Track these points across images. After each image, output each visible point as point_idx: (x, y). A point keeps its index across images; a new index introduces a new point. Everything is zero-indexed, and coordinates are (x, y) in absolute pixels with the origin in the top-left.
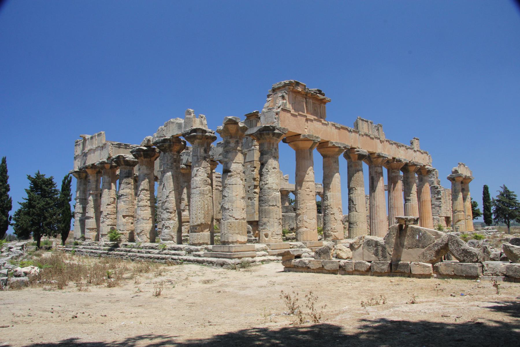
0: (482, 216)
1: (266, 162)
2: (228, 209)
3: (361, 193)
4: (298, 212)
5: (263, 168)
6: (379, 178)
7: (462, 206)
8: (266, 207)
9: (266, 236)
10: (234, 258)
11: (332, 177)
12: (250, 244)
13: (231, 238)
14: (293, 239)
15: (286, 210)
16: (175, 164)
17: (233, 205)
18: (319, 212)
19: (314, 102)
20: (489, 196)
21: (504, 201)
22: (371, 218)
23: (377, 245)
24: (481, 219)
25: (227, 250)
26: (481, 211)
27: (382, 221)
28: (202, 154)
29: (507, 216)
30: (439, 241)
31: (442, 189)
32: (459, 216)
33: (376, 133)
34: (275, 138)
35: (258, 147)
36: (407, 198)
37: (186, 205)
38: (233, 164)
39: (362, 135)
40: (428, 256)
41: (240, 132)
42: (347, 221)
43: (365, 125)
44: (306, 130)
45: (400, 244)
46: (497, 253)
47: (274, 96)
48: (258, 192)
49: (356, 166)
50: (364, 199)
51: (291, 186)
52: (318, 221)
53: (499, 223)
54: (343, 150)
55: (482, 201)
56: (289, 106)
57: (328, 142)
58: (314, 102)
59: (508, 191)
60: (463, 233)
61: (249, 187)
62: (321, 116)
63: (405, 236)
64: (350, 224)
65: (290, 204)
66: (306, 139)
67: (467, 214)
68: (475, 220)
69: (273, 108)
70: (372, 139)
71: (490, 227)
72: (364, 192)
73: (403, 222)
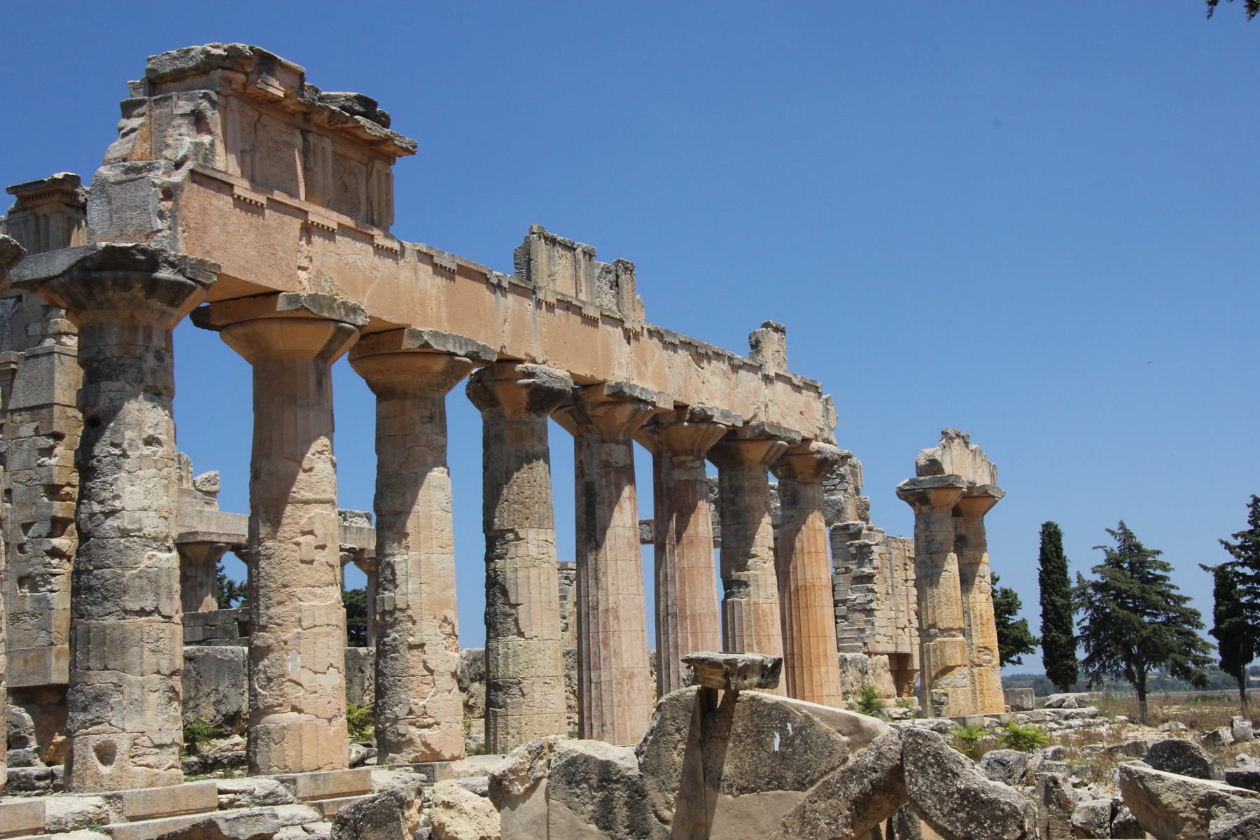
0: (1039, 650)
1: (114, 411)
3: (543, 550)
4: (261, 639)
5: (97, 439)
6: (619, 491)
7: (957, 611)
8: (110, 621)
12: (18, 800)
14: (236, 763)
15: (203, 630)
18: (356, 636)
20: (1063, 569)
21: (1124, 587)
22: (583, 662)
23: (609, 781)
24: (1033, 663)
26: (1035, 629)
27: (631, 676)
29: (1135, 650)
31: (879, 538)
32: (948, 651)
33: (608, 300)
34: (157, 304)
35: (72, 342)
36: (735, 574)
39: (550, 307)
40: (822, 824)
42: (480, 677)
43: (563, 263)
44: (302, 275)
45: (706, 770)
46: (1097, 804)
47: (157, 112)
48: (72, 552)
49: (520, 437)
50: (555, 579)
51: (228, 521)
52: (349, 681)
53: (1105, 679)
54: (469, 367)
55: (1038, 588)
56: (225, 163)
57: (399, 330)
58: (341, 149)
59: (1138, 547)
60: (962, 721)
61: (26, 527)
62: (370, 213)
64: (490, 689)
65: (224, 603)
66: (305, 314)
67: (977, 641)
68: (1010, 669)
69: (151, 168)
70: (592, 322)
71: (1071, 697)
72: (552, 550)
73: (718, 678)
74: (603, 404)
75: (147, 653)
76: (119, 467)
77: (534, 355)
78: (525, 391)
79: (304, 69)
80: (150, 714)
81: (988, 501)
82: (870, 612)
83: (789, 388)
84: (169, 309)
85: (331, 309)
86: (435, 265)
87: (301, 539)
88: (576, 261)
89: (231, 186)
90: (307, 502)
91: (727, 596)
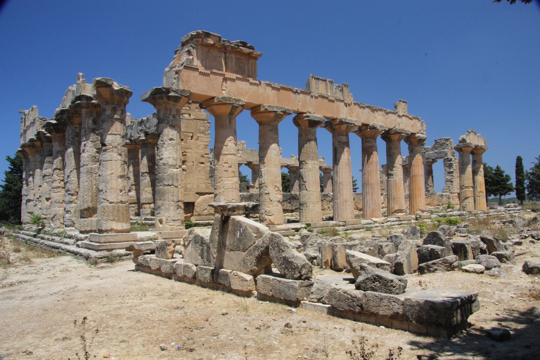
2: (102, 191)
6: (344, 149)
8: (161, 187)
9: (161, 222)
10: (101, 250)
11: (267, 148)
16: (77, 138)
17: (107, 185)
19: (238, 57)
20: (522, 169)
25: (98, 241)
27: (346, 201)
28: (90, 125)
30: (259, 242)
32: (467, 193)
33: (339, 95)
36: (390, 172)
37: (132, 185)
38: (108, 136)
39: (316, 98)
40: (249, 264)
43: (322, 85)
44: (223, 92)
56: (197, 63)
58: (238, 57)
63: (227, 232)
74: (338, 124)
75: (170, 196)
77: (310, 111)
78: (307, 122)
80: (171, 212)
81: (482, 150)
82: (452, 182)
83: (408, 119)
84: (176, 104)
85: (230, 100)
86: (272, 87)
88: (327, 84)
89: (198, 69)
90: (226, 155)
91: (388, 178)
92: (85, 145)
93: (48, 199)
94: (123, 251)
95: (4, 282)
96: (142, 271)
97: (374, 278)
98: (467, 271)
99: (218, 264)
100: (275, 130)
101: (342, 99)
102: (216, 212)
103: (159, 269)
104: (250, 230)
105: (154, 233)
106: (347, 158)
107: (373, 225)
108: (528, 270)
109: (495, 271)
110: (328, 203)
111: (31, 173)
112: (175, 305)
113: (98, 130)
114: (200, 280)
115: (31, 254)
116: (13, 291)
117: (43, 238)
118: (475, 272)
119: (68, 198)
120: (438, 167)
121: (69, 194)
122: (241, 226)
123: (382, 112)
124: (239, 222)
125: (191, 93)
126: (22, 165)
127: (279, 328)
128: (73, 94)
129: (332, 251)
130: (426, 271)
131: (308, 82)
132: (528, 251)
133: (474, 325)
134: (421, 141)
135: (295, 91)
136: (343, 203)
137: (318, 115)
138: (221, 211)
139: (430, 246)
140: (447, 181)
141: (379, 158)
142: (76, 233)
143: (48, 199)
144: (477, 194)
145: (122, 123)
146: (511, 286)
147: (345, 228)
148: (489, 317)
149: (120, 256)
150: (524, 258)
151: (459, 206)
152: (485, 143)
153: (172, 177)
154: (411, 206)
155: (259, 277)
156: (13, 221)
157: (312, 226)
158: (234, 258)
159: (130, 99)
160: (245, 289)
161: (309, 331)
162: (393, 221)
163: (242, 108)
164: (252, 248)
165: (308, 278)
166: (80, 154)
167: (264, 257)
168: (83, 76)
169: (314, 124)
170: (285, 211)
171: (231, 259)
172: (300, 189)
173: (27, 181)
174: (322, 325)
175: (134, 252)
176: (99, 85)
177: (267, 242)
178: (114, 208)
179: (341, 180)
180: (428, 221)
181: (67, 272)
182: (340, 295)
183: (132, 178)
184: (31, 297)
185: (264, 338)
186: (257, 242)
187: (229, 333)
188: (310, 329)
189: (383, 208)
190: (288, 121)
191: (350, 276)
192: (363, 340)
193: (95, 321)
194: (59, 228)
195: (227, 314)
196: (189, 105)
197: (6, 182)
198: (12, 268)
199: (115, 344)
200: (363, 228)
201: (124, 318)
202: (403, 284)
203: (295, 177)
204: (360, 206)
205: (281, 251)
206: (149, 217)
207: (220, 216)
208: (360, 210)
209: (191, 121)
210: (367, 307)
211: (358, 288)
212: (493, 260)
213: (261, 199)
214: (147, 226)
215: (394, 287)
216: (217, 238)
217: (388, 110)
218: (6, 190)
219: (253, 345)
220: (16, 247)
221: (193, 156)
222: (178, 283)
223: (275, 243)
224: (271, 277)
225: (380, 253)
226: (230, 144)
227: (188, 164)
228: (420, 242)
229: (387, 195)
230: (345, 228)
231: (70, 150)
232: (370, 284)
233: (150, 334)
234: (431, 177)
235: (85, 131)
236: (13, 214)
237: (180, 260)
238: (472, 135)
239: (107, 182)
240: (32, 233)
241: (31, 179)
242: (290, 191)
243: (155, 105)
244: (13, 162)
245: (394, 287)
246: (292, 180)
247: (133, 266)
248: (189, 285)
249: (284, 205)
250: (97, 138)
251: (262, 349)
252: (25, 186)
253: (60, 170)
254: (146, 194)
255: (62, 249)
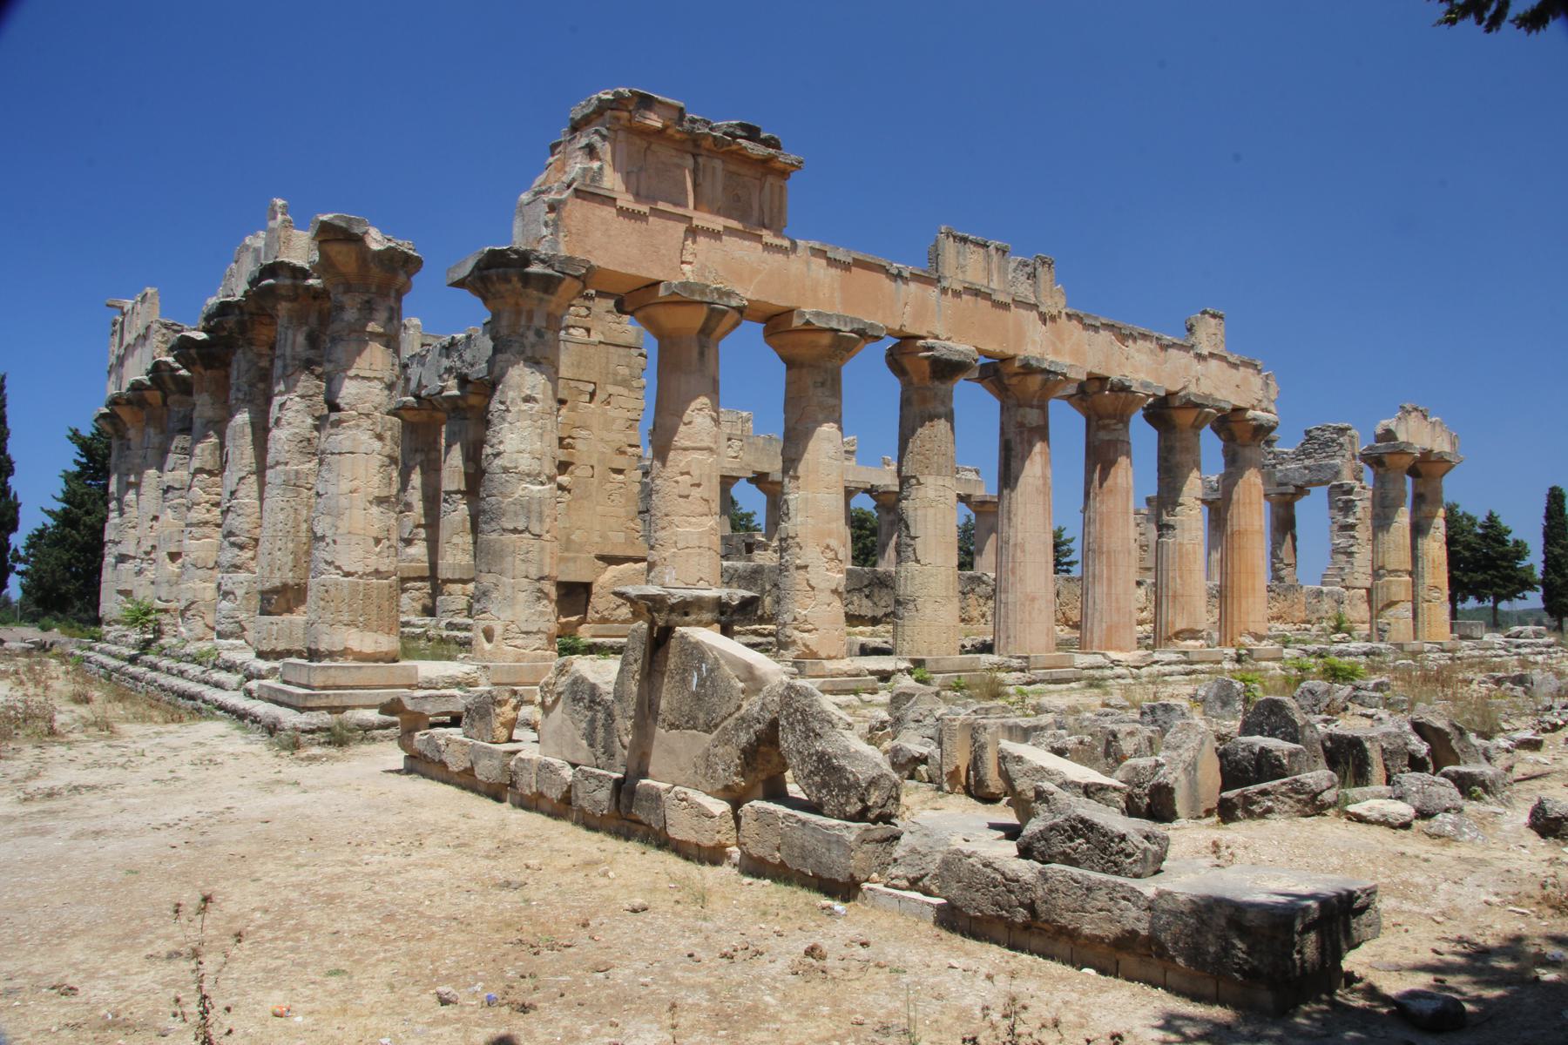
2: (323, 538)
6: (1031, 446)
8: (494, 536)
9: (489, 635)
10: (311, 709)
11: (807, 435)
13: (326, 637)
16: (261, 386)
17: (339, 523)
19: (732, 168)
25: (304, 681)
27: (1033, 599)
28: (299, 349)
32: (1393, 589)
33: (1024, 290)
36: (1165, 518)
37: (418, 526)
38: (347, 382)
39: (957, 294)
40: (720, 768)
41: (375, 271)
43: (974, 257)
44: (686, 268)
49: (924, 400)
56: (612, 181)
57: (790, 311)
58: (732, 168)
63: (663, 674)
74: (1017, 374)
75: (518, 562)
76: (504, 419)
77: (937, 332)
78: (926, 363)
79: (682, 105)
81: (1445, 466)
82: (1351, 554)
84: (546, 297)
85: (703, 293)
86: (828, 259)
87: (679, 478)
88: (989, 256)
90: (686, 449)
91: (1160, 536)
92: (282, 406)
93: (174, 557)
94: (373, 716)
95: (32, 786)
96: (424, 775)
97: (1072, 827)
98: (1360, 819)
99: (634, 765)
100: (833, 384)
101: (1033, 300)
102: (636, 615)
103: (469, 771)
104: (727, 670)
105: (467, 668)
106: (1039, 473)
107: (1107, 672)
108: (1547, 825)
109: (1444, 822)
110: (982, 601)
111: (132, 479)
112: (501, 876)
113: (320, 364)
114: (582, 809)
115: (118, 709)
116: (53, 813)
117: (154, 667)
118: (1385, 822)
119: (229, 555)
120: (1312, 512)
121: (233, 544)
122: (702, 658)
123: (1148, 344)
124: (697, 646)
125: (591, 269)
126: (110, 455)
127: (789, 958)
128: (257, 259)
129: (971, 742)
130: (1239, 813)
131: (936, 246)
132: (1557, 767)
133: (1361, 980)
134: (1262, 432)
135: (895, 272)
136: (1023, 604)
137: (959, 346)
138: (649, 610)
139: (1260, 741)
140: (1336, 551)
141: (1134, 476)
142: (247, 657)
143: (174, 557)
144: (1423, 592)
145: (387, 346)
146: (1488, 870)
147: (1027, 676)
148: (1411, 959)
149: (366, 728)
150: (1543, 788)
151: (1367, 626)
152: (1453, 444)
153: (526, 507)
154: (1224, 622)
155: (746, 806)
156: (83, 615)
157: (930, 666)
158: (689, 751)
159: (414, 279)
160: (706, 841)
161: (873, 970)
162: (1169, 664)
163: (737, 315)
164: (730, 722)
165: (886, 819)
166: (267, 430)
167: (763, 749)
168: (286, 210)
169: (946, 369)
170: (853, 619)
171: (671, 751)
172: (900, 559)
173: (120, 500)
174: (913, 957)
175: (404, 720)
176: (328, 235)
177: (774, 707)
178: (354, 590)
179: (1020, 536)
180: (1274, 668)
181: (211, 767)
182: (973, 871)
183: (418, 506)
184: (97, 833)
185: (740, 984)
186: (745, 705)
187: (640, 965)
188: (878, 966)
189: (1140, 623)
190: (872, 358)
191: (1010, 818)
192: (1014, 1008)
193: (266, 911)
194: (200, 639)
195: (645, 909)
196: (587, 303)
197: (66, 501)
198: (57, 748)
199: (313, 977)
200: (1078, 680)
201: (350, 906)
202: (1155, 848)
203: (892, 524)
204: (1075, 616)
205: (811, 734)
206: (458, 620)
207: (646, 626)
208: (1076, 626)
209: (592, 350)
210: (1048, 912)
211: (1025, 852)
212: (1441, 790)
213: (785, 582)
214: (453, 647)
215: (1129, 856)
216: (635, 689)
217: (1168, 338)
218: (65, 526)
219: (705, 1004)
220: (78, 687)
221: (590, 449)
222: (521, 814)
223: (796, 711)
224: (781, 810)
225: (1109, 751)
226: (698, 420)
227: (577, 472)
228: (1232, 725)
229: (1155, 584)
230: (1027, 676)
231: (242, 418)
232: (1059, 845)
233: (415, 957)
234: (1289, 537)
235: (285, 367)
236: (80, 595)
237: (529, 749)
238: (1414, 420)
239: (339, 516)
240: (127, 652)
241: (130, 496)
242: (874, 565)
243: (485, 300)
244: (86, 447)
245: (1129, 856)
246: (884, 529)
247: (397, 758)
248: (550, 822)
249: (851, 603)
250: (318, 387)
251: (729, 1016)
252: (112, 515)
253: (210, 473)
254: (456, 554)
255: (205, 701)
